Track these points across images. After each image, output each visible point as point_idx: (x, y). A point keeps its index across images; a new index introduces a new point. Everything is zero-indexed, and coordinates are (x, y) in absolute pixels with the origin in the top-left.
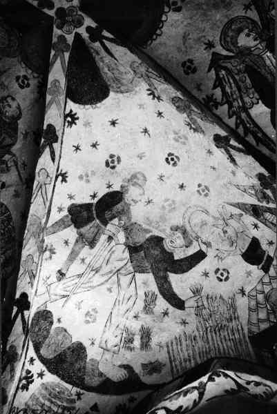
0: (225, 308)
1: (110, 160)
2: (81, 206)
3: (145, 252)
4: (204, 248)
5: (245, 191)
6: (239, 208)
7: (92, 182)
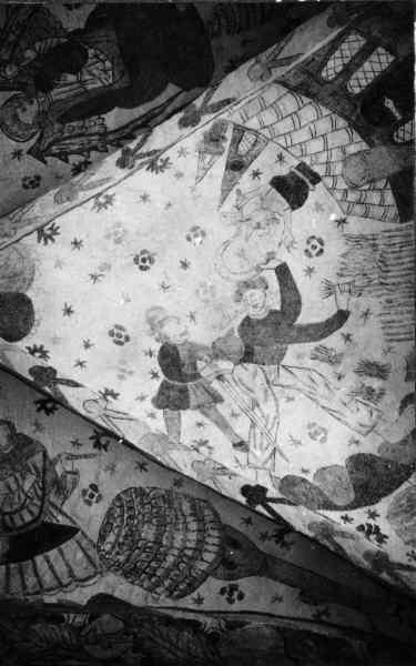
0: (359, 252)
1: (115, 338)
2: (161, 392)
3: (257, 345)
4: (274, 264)
5: (207, 170)
6: (230, 190)
7: (134, 368)
